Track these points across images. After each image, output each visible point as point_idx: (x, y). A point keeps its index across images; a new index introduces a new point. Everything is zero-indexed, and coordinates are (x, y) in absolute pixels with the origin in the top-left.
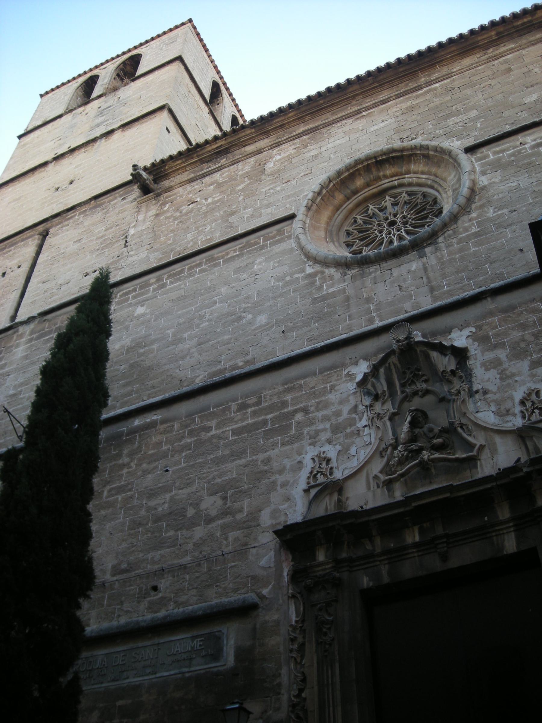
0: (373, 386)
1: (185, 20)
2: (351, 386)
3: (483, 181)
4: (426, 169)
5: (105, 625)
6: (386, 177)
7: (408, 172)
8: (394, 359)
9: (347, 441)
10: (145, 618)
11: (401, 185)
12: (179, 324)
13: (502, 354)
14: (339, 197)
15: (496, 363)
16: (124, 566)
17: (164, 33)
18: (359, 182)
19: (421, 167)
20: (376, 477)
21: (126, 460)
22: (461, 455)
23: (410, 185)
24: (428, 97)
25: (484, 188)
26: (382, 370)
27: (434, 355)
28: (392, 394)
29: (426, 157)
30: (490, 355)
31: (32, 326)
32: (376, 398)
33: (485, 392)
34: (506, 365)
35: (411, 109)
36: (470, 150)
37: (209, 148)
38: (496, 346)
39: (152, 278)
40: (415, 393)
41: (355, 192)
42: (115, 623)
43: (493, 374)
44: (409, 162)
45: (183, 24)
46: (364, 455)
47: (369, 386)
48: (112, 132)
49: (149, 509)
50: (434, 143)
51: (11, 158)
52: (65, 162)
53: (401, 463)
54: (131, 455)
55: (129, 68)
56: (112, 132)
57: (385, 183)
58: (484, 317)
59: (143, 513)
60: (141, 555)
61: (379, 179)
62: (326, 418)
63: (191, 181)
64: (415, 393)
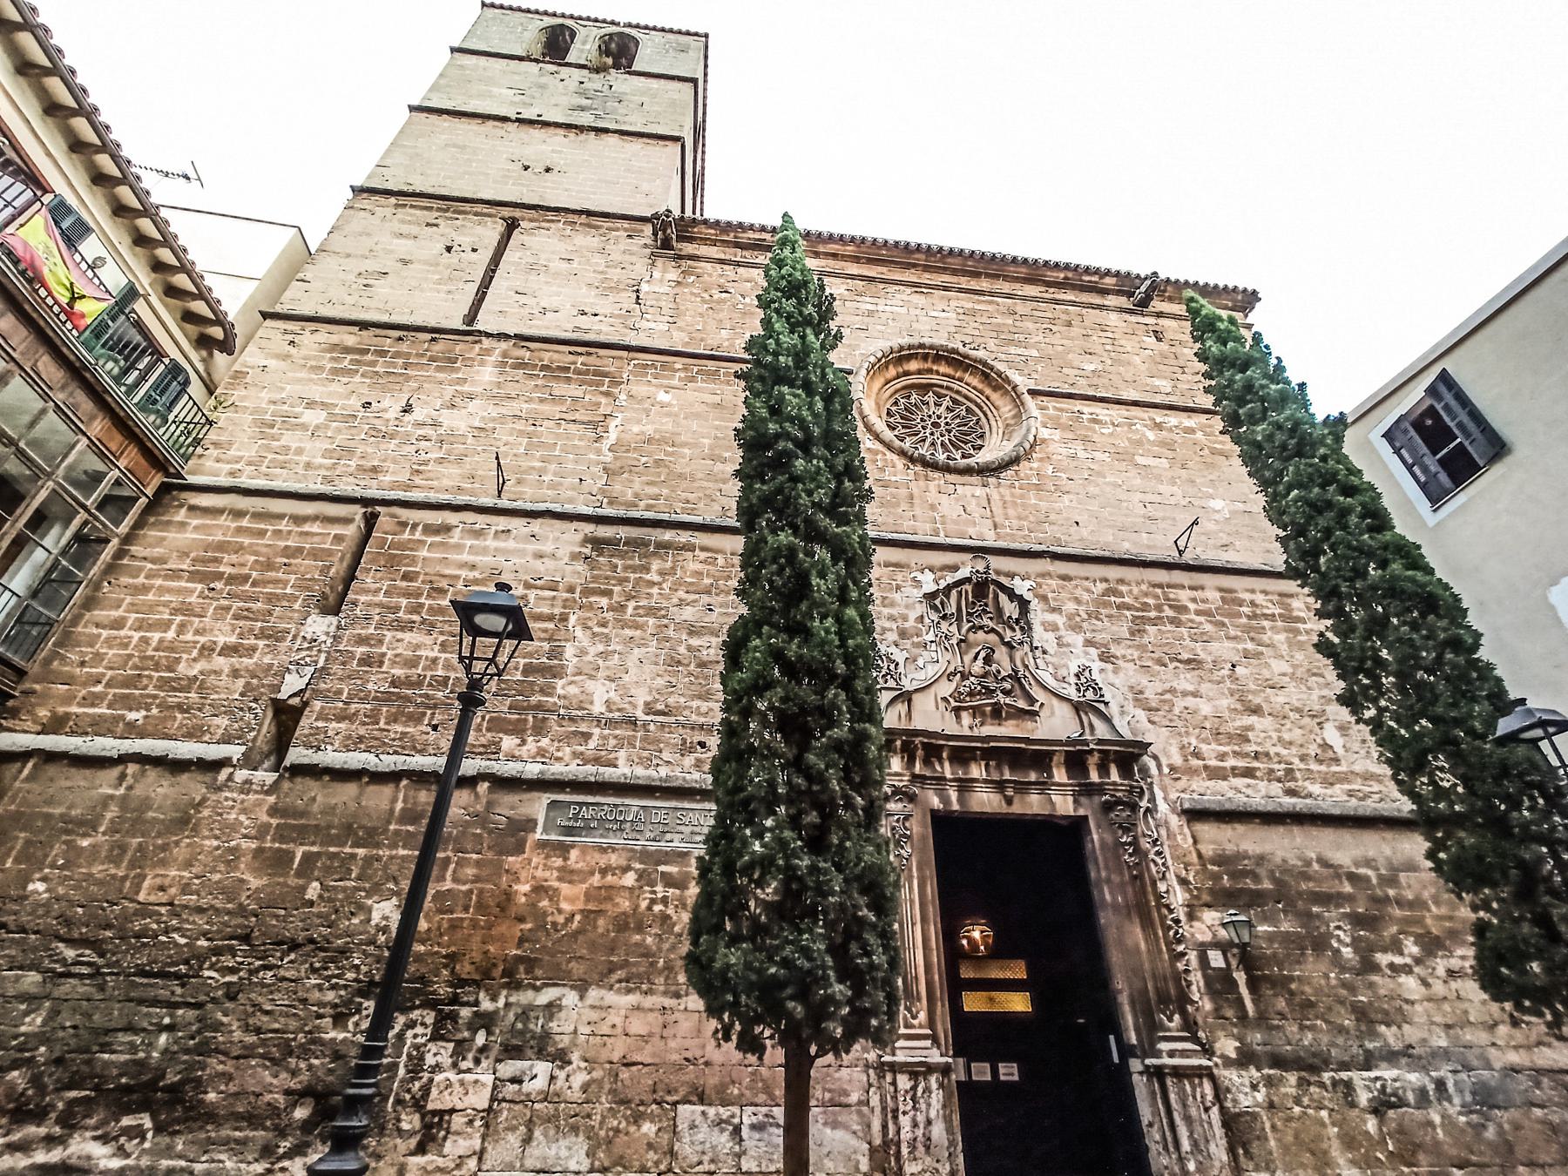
0: (942, 603)
1: (701, 31)
2: (918, 594)
3: (1044, 433)
4: (980, 386)
5: (640, 771)
6: (938, 373)
7: (960, 380)
8: (969, 587)
9: (916, 651)
10: (688, 777)
11: (948, 388)
12: (716, 437)
13: (1060, 620)
14: (892, 372)
15: (1054, 628)
16: (660, 707)
17: (671, 31)
18: (913, 366)
19: (975, 382)
20: (944, 699)
21: (656, 578)
22: (1022, 704)
23: (958, 392)
24: (990, 308)
25: (1044, 441)
26: (954, 591)
27: (1003, 598)
28: (959, 619)
29: (986, 376)
30: (1050, 617)
31: (504, 345)
32: (944, 617)
33: (1044, 652)
34: (1063, 633)
35: (972, 313)
36: (1032, 393)
37: (751, 234)
38: (1054, 610)
39: (679, 363)
40: (981, 628)
41: (907, 373)
42: (651, 772)
43: (1051, 636)
44: (965, 371)
45: (696, 34)
46: (932, 671)
47: (937, 602)
48: (606, 131)
49: (689, 648)
50: (1000, 367)
51: (441, 75)
52: (536, 133)
53: (971, 694)
54: (661, 573)
55: (619, 51)
56: (606, 131)
57: (934, 379)
58: (1043, 575)
59: (682, 650)
60: (682, 700)
61: (930, 371)
62: (891, 618)
63: (722, 262)
64: (981, 628)
